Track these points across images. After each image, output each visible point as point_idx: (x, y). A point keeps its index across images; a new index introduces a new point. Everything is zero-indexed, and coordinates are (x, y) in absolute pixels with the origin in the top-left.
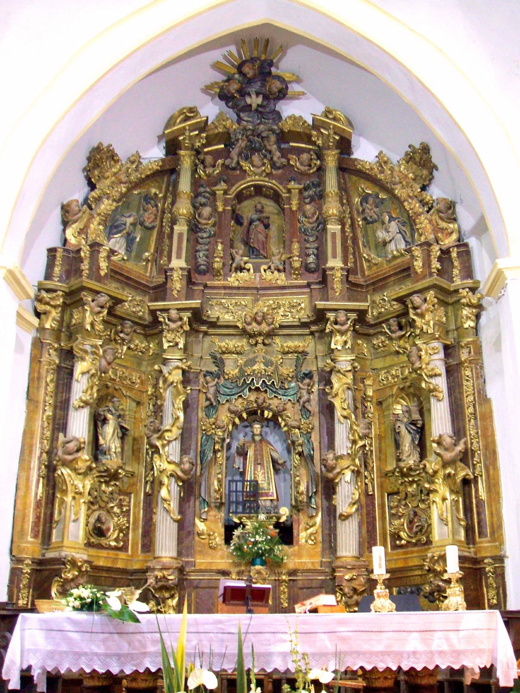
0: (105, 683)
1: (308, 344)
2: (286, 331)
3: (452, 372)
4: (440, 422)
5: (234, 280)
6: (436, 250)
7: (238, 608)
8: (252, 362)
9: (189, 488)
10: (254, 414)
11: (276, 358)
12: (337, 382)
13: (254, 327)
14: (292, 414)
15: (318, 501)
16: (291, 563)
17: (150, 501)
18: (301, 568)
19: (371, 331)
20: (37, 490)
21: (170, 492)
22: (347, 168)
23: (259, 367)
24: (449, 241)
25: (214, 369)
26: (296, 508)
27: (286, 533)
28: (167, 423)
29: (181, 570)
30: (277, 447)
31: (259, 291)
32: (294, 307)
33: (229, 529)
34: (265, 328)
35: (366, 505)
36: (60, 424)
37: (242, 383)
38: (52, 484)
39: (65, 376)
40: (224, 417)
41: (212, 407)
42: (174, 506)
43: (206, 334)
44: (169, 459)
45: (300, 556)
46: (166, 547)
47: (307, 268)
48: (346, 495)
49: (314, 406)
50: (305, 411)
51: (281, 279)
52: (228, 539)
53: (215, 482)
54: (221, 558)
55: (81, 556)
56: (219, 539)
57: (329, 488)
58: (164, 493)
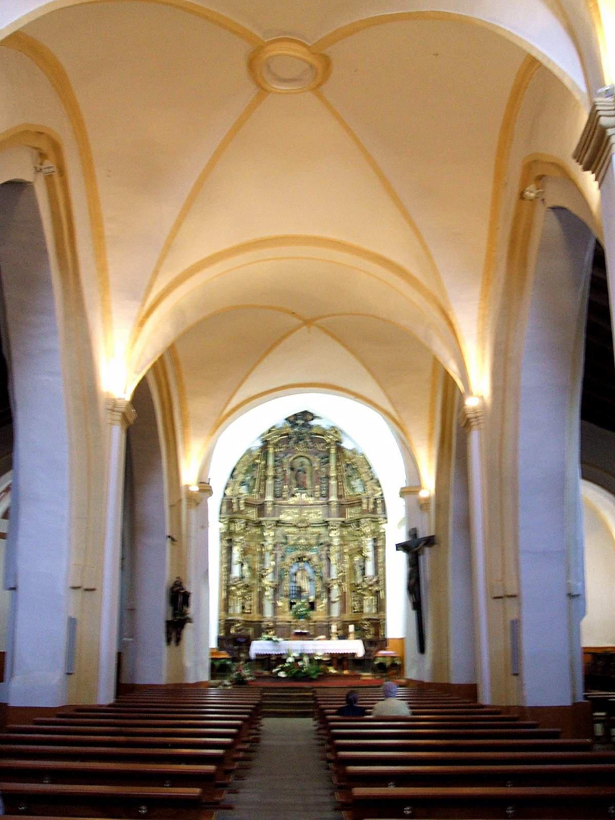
0: (328, 659)
1: (322, 530)
2: (312, 525)
3: (376, 548)
4: (370, 566)
5: (292, 501)
6: (372, 500)
7: (26, 22)
8: (299, 539)
9: (276, 590)
10: (300, 559)
11: (308, 536)
12: (332, 549)
13: (300, 525)
14: (315, 559)
15: (324, 594)
16: (315, 618)
17: (261, 595)
18: (318, 620)
19: (347, 525)
20: (224, 594)
21: (269, 593)
22: (340, 449)
23: (302, 541)
24: (377, 495)
25: (284, 541)
26: (317, 597)
27: (312, 606)
28: (267, 566)
29: (274, 622)
30: (309, 570)
31: (302, 506)
32: (315, 515)
33: (292, 604)
34: (304, 525)
35: (343, 597)
36: (229, 570)
37: (295, 547)
38: (229, 592)
39: (230, 550)
40: (288, 560)
41: (283, 557)
42: (270, 597)
43: (280, 526)
44: (268, 581)
45: (317, 615)
46: (268, 613)
47: (322, 496)
48: (335, 593)
49: (324, 557)
50: (320, 559)
51: (311, 500)
52: (291, 608)
53: (287, 587)
54: (288, 616)
55: (240, 618)
56: (287, 609)
57: (329, 591)
58: (266, 593)
